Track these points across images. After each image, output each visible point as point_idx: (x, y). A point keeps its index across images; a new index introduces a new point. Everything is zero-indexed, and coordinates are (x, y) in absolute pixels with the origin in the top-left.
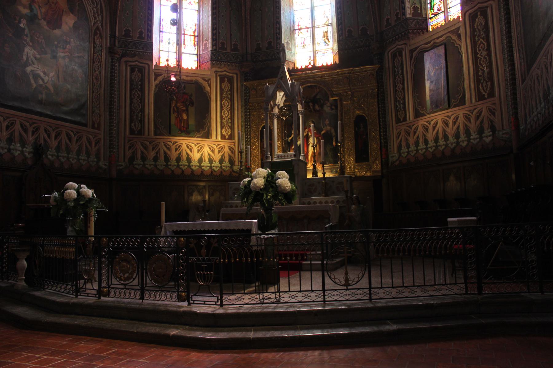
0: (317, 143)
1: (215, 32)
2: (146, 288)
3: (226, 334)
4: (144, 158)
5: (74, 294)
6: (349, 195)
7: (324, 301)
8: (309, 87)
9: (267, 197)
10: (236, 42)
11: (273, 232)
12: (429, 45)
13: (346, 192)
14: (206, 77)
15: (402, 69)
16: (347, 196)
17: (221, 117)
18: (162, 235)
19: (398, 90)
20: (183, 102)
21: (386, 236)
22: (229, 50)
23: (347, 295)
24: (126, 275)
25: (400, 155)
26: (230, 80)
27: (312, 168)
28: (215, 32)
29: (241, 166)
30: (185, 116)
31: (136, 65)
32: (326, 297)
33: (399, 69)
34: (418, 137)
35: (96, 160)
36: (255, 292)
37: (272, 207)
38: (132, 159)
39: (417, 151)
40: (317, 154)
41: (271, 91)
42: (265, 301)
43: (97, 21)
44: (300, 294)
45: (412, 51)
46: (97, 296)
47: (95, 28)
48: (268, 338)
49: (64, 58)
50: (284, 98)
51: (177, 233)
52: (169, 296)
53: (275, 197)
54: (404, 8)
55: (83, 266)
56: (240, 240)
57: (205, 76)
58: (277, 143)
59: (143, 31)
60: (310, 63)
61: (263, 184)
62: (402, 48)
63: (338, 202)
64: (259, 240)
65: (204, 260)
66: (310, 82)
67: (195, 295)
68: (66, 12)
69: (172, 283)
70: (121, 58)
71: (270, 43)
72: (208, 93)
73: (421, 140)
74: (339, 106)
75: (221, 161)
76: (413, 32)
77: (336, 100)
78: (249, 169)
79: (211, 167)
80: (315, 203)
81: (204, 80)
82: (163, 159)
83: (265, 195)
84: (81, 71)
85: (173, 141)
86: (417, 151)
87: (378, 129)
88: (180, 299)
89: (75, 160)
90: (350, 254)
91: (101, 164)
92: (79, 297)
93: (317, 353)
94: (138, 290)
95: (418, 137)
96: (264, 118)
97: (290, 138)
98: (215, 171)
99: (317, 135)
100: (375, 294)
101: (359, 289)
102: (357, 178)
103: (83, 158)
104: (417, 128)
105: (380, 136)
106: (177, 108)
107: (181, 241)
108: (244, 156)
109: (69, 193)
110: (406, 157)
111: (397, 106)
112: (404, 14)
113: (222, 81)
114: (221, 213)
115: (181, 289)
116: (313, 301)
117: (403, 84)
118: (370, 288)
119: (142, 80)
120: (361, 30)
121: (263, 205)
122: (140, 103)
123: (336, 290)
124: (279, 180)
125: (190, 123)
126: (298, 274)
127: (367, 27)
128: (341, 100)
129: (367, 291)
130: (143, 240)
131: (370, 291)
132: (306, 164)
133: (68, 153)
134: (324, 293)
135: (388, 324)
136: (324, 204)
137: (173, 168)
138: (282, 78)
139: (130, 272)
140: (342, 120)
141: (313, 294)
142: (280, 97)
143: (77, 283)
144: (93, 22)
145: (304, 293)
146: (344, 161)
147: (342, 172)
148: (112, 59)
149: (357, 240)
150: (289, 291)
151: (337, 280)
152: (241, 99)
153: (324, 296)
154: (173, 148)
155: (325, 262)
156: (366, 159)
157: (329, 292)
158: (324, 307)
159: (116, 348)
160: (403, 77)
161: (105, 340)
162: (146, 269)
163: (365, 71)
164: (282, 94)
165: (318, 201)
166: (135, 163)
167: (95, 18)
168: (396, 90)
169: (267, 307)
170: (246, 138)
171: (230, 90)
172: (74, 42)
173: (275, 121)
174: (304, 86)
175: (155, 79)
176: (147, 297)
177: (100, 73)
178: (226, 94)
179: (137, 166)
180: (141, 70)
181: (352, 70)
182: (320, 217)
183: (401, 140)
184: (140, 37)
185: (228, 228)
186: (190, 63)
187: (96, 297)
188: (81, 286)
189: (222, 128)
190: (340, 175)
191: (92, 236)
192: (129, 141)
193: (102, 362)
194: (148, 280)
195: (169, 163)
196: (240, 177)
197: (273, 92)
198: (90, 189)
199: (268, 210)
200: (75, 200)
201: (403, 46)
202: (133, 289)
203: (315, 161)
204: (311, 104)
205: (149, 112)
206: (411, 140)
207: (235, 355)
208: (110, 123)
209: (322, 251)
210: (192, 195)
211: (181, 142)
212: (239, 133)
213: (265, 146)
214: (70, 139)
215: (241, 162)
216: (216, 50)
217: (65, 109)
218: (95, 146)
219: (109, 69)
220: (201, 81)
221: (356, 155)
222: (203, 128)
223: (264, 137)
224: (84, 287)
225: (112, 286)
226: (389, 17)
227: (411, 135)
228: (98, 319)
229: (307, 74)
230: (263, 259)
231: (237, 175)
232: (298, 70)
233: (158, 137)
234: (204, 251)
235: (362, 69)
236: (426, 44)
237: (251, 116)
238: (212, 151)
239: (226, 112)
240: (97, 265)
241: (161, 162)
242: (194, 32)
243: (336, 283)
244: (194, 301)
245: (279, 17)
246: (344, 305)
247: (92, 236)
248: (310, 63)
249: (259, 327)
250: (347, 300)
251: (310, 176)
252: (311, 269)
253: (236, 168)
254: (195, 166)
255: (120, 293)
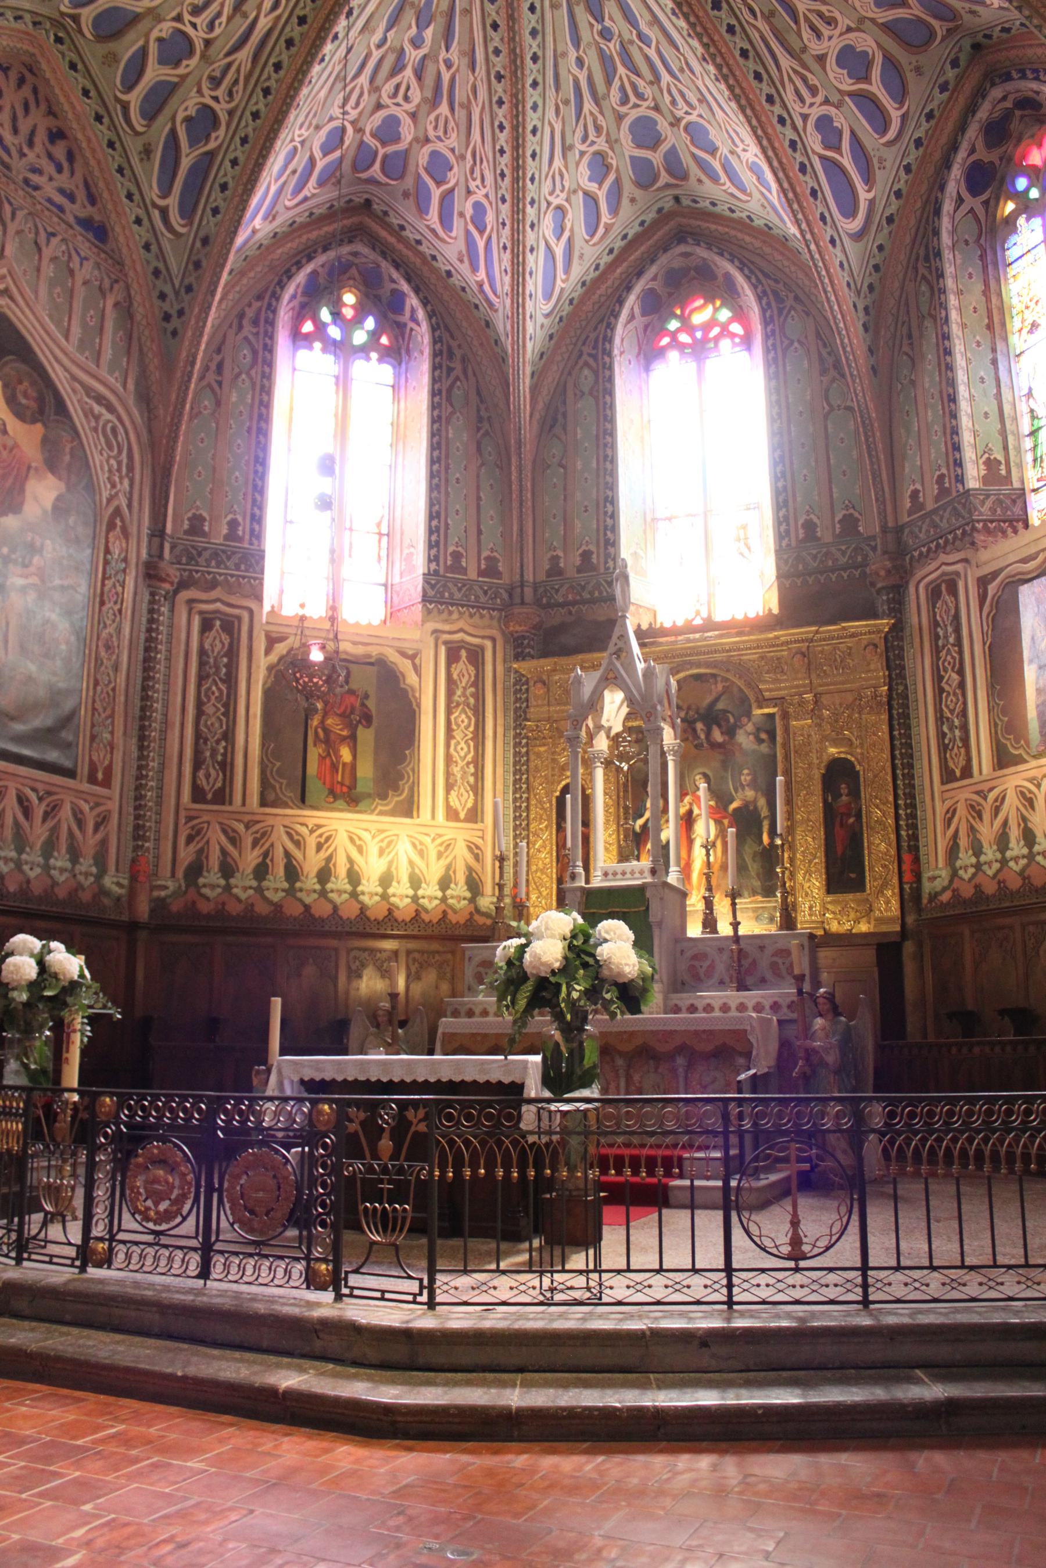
0: (717, 837)
1: (435, 523)
2: (218, 1246)
3: (439, 1390)
4: (228, 870)
5: (13, 1254)
6: (807, 987)
7: (730, 1303)
8: (698, 677)
9: (569, 994)
10: (492, 550)
11: (585, 1093)
12: (1032, 565)
13: (800, 979)
14: (409, 648)
15: (958, 630)
16: (800, 992)
17: (449, 759)
18: (269, 1093)
19: (947, 688)
20: (342, 721)
21: (912, 1115)
22: (473, 574)
23: (797, 1285)
24: (163, 1206)
25: (954, 874)
26: (476, 657)
27: (701, 906)
28: (435, 523)
29: (500, 898)
30: (346, 754)
31: (217, 611)
32: (735, 1290)
33: (950, 629)
34: (1005, 823)
35: (94, 870)
36: (530, 1268)
37: (585, 1020)
38: (195, 870)
39: (1004, 862)
40: (716, 868)
41: (587, 690)
42: (559, 1297)
43: (117, 494)
44: (658, 1280)
45: (983, 582)
46: (78, 1263)
47: (111, 510)
48: (563, 1409)
49: (23, 590)
50: (625, 710)
51: (315, 1087)
52: (280, 1272)
53: (592, 994)
54: (959, 464)
55: (42, 1172)
56: (489, 1117)
57: (406, 645)
58: (603, 835)
59: (240, 519)
60: (698, 613)
61: (559, 956)
62: (957, 574)
63: (775, 1007)
64: (545, 1115)
65: (385, 1170)
66: (699, 665)
67: (356, 1271)
68: (36, 469)
69: (292, 1233)
70: (176, 592)
71: (586, 555)
72: (413, 690)
73: (1014, 833)
74: (779, 732)
75: (445, 883)
76: (985, 527)
77: (771, 716)
78: (521, 911)
79: (415, 899)
80: (709, 1008)
81: (403, 654)
82: (281, 871)
83: (564, 988)
84: (67, 625)
85: (311, 823)
86: (1004, 862)
87: (891, 798)
88: (312, 1281)
89: (38, 870)
90: (806, 1166)
91: (108, 882)
92: (25, 1264)
93: (704, 1462)
94: (195, 1249)
95: (1005, 823)
96: (567, 764)
97: (640, 822)
98: (426, 911)
99: (719, 812)
100: (879, 1285)
101: (831, 1270)
102: (830, 940)
103: (59, 864)
104: (1002, 799)
105: (897, 817)
106: (327, 731)
107: (321, 1112)
108: (509, 870)
109: (15, 965)
110: (970, 880)
111: (944, 735)
112: (960, 479)
113: (452, 657)
114: (440, 1031)
115: (318, 1252)
116: (698, 1303)
117: (961, 672)
118: (864, 1268)
119: (232, 653)
120: (840, 522)
121: (559, 1016)
122: (223, 714)
123: (763, 1270)
124: (605, 945)
125: (359, 774)
126: (656, 1215)
127: (856, 515)
128: (785, 716)
129: (856, 1276)
130: (216, 1106)
131: (865, 1277)
132: (684, 895)
133: (20, 850)
134: (729, 1278)
135: (918, 1381)
136: (734, 1013)
137: (308, 900)
138: (618, 653)
139: (173, 1197)
140: (787, 773)
141: (697, 1280)
142: (614, 709)
143: (21, 1224)
144: (105, 494)
145: (670, 1275)
146: (793, 888)
147: (788, 921)
148: (152, 594)
149: (828, 1124)
150: (629, 1270)
151: (767, 1243)
152: (506, 710)
153: (730, 1286)
154: (312, 842)
155: (733, 1183)
156: (858, 885)
157: (744, 1275)
158: (728, 1320)
159: (123, 1421)
160: (961, 652)
161: (91, 1396)
162: (220, 1191)
163: (853, 635)
164: (620, 696)
165: (716, 1004)
166: (201, 881)
167: (113, 486)
168: (941, 690)
169: (561, 1316)
170: (515, 818)
171: (475, 684)
172: (53, 549)
173: (599, 773)
174: (682, 675)
175: (268, 651)
176: (217, 1271)
177: (119, 630)
178: (464, 694)
179: (206, 891)
180: (230, 626)
181: (817, 632)
182: (725, 1049)
183: (957, 831)
184: (232, 535)
185: (457, 1078)
186: (364, 610)
187: (72, 1266)
188: (33, 1232)
189: (449, 787)
190: (781, 928)
191: (72, 1090)
192: (190, 819)
193: (78, 1465)
194: (224, 1222)
195: (298, 885)
196: (491, 930)
197: (594, 692)
198: (74, 955)
199: (573, 1029)
200: (34, 986)
201: (959, 567)
202: (181, 1248)
203: (709, 889)
204: (699, 726)
205: (247, 741)
206: (987, 832)
207: (465, 1458)
208: (140, 768)
209: (726, 1149)
210: (360, 977)
211: (334, 825)
212: (495, 805)
213: (569, 844)
214: (27, 812)
215: (501, 887)
216: (436, 573)
217: (19, 727)
218: (96, 829)
219: (144, 620)
220: (393, 657)
221: (827, 873)
222: (396, 789)
223: (568, 809)
224: (42, 1235)
225: (121, 1236)
226: (919, 487)
227: (986, 816)
228: (75, 1331)
229: (689, 641)
230: (554, 1170)
231: (489, 922)
232: (664, 632)
233: (268, 810)
234: (386, 1144)
235: (844, 628)
236: (1024, 561)
237: (532, 757)
238: (421, 853)
239: (463, 744)
240: (81, 1171)
241: (276, 881)
242: (379, 525)
243: (764, 1249)
244: (352, 1288)
245: (612, 486)
246: (789, 1315)
247: (72, 1090)
248: (698, 613)
249: (537, 1375)
250: (797, 1302)
251: (694, 930)
252: (692, 1203)
253: (487, 902)
254: (372, 895)
255: (142, 1257)
